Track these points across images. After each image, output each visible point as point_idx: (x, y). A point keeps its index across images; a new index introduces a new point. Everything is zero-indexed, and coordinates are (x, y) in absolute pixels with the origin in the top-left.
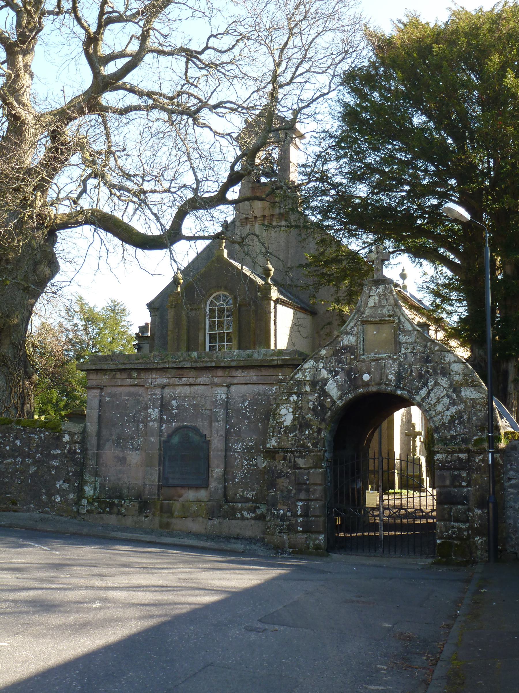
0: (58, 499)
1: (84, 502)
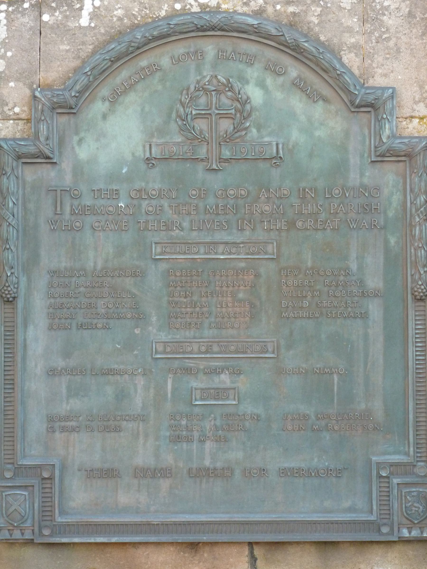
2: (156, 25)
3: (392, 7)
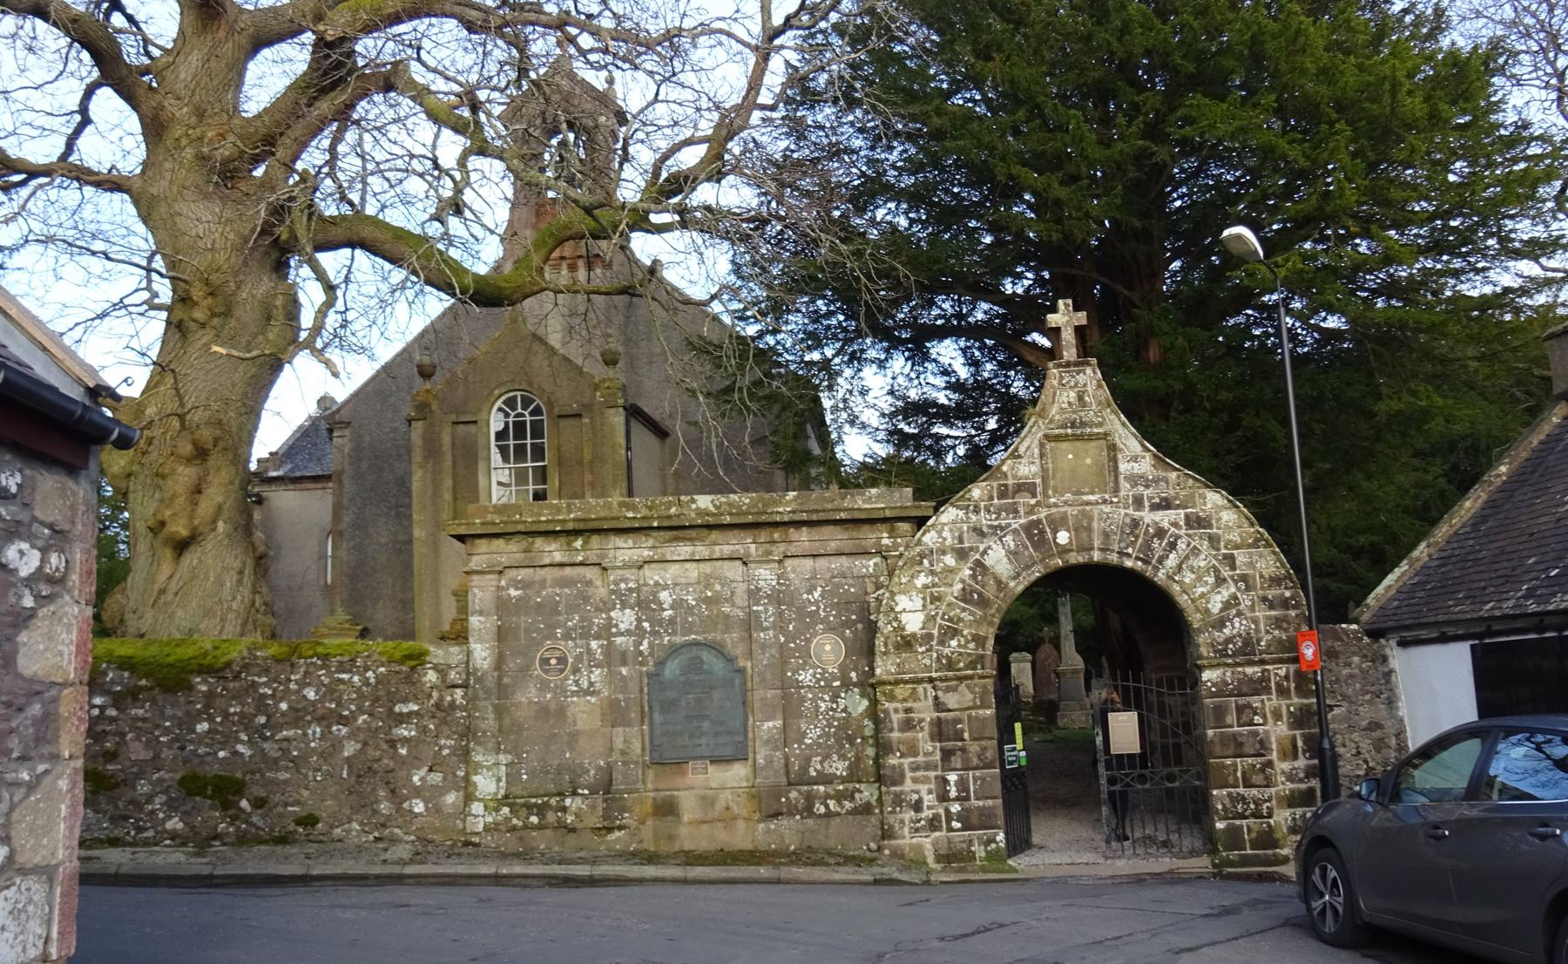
0: (419, 807)
1: (477, 808)
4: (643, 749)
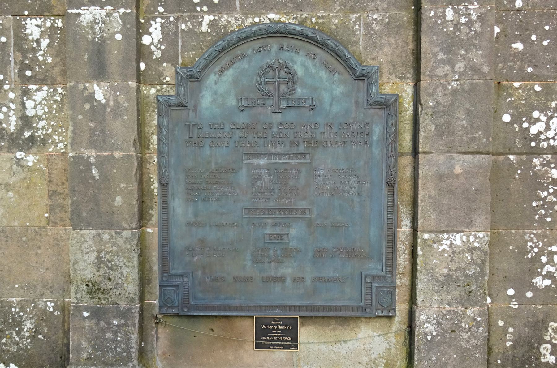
2: (244, 30)
3: (378, 19)
4: (143, 282)
